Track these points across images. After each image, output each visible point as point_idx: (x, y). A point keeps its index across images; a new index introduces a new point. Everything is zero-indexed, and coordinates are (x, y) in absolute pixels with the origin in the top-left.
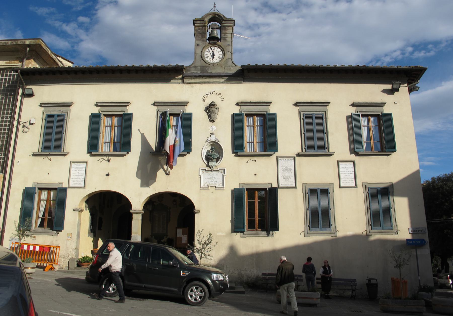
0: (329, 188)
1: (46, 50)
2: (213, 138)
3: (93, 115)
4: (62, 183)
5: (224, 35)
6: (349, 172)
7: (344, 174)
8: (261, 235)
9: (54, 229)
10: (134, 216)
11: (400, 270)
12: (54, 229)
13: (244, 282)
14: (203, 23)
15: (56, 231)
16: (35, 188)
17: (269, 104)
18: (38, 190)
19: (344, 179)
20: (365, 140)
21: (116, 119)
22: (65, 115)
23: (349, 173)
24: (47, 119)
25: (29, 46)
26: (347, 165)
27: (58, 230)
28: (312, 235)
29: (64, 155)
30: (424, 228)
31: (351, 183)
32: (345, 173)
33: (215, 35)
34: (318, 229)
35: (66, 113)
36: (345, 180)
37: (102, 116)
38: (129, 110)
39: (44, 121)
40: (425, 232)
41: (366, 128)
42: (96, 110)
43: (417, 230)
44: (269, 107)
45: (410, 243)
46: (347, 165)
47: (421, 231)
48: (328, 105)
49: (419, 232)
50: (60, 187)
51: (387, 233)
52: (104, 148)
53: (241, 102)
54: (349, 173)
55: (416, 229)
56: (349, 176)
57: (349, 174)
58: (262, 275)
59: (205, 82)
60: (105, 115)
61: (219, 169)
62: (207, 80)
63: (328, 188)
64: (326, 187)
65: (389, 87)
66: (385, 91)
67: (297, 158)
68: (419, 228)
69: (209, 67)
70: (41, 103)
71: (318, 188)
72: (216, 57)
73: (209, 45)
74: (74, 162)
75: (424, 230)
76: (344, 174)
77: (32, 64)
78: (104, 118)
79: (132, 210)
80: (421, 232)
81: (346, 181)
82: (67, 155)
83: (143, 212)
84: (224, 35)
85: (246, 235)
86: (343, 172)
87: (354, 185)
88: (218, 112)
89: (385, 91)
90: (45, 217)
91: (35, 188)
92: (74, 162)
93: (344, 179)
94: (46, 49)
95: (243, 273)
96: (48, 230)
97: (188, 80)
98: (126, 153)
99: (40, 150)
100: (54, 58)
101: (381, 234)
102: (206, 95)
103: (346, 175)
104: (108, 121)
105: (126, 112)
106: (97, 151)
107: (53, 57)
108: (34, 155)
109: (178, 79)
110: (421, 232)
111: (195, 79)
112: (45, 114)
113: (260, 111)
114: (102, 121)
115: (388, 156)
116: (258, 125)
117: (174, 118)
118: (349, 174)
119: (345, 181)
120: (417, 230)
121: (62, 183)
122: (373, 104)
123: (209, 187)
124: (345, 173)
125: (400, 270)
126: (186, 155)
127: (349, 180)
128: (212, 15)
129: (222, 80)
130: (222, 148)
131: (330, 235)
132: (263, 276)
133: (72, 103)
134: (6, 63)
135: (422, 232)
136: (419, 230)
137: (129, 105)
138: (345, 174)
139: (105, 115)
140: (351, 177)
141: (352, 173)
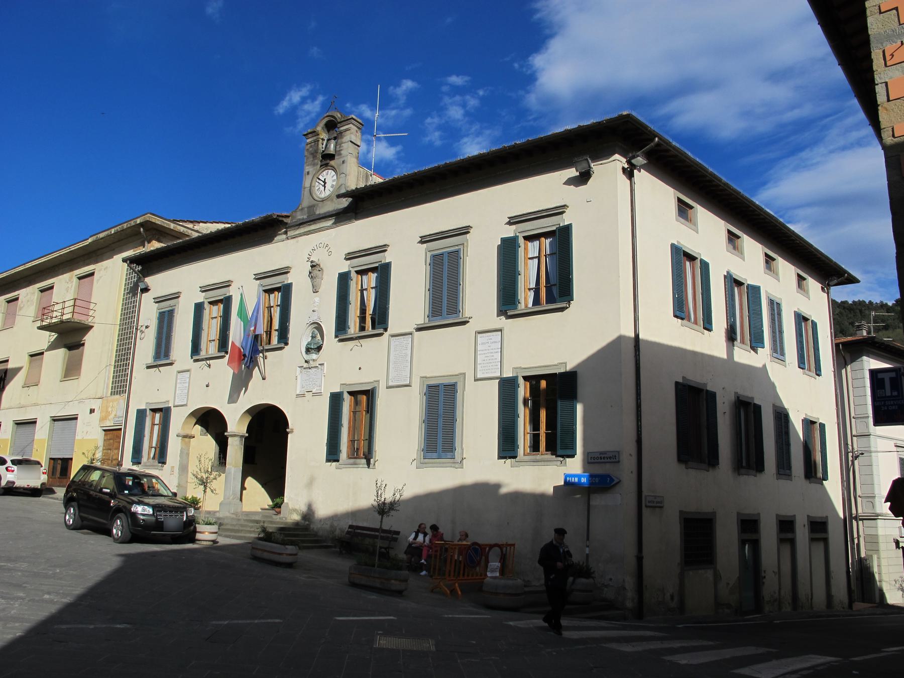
0: (457, 382)
1: (162, 224)
2: (314, 318)
3: (504, 240)
4: (566, 363)
5: (340, 147)
6: (492, 349)
7: (484, 354)
8: (361, 466)
9: (558, 454)
10: (230, 440)
11: (382, 519)
12: (558, 454)
13: (337, 538)
14: (315, 136)
15: (562, 456)
16: (517, 377)
17: (286, 271)
18: (349, 396)
19: (483, 364)
20: (277, 328)
21: (547, 242)
22: (460, 251)
23: (492, 353)
24: (432, 264)
25: (141, 225)
26: (490, 338)
27: (565, 455)
28: (427, 465)
29: (464, 323)
30: (617, 451)
31: (493, 371)
32: (485, 352)
33: (330, 151)
34: (435, 455)
35: (461, 247)
36: (485, 365)
37: (521, 241)
38: (565, 219)
39: (428, 267)
40: (617, 460)
41: (536, 261)
42: (510, 232)
43: (603, 456)
44: (386, 253)
45: (573, 480)
46: (490, 338)
47: (610, 458)
48: (468, 232)
49: (606, 460)
50: (562, 371)
51: (546, 463)
52: (526, 298)
53: (348, 253)
54: (492, 353)
55: (600, 454)
56: (493, 358)
57: (492, 355)
58: (349, 528)
59: (310, 231)
60: (526, 238)
61: (318, 365)
62: (313, 227)
63: (455, 383)
64: (452, 381)
65: (572, 172)
66: (571, 182)
67: (416, 334)
68: (605, 453)
69: (318, 205)
70: (509, 218)
71: (440, 384)
72: (328, 186)
73: (320, 170)
74: (480, 333)
75: (615, 456)
76: (484, 354)
77: (155, 245)
78: (525, 243)
79: (227, 432)
80: (609, 460)
81: (486, 368)
82: (468, 322)
83: (247, 435)
84: (340, 147)
85: (343, 466)
86: (483, 350)
87: (479, 376)
88: (322, 275)
89: (571, 182)
90: (534, 434)
91: (517, 377)
92: (480, 333)
93: (483, 364)
94: (164, 223)
95: (335, 524)
96: (549, 456)
97: (292, 232)
98: (381, 331)
99: (427, 319)
100: (184, 231)
101: (535, 464)
102: (312, 251)
103: (487, 357)
104: (533, 248)
105: (561, 225)
106: (346, 333)
107: (182, 231)
108: (148, 367)
109: (281, 234)
110: (609, 460)
111: (299, 229)
112: (429, 255)
113: (374, 262)
114: (521, 251)
115: (562, 311)
116: (279, 303)
117: (547, 240)
118: (492, 355)
119: (484, 368)
120: (601, 455)
121: (566, 363)
122: (543, 213)
123: (306, 393)
124: (485, 352)
125: (382, 519)
126: (284, 348)
127: (490, 365)
128: (326, 118)
129: (330, 223)
130: (323, 331)
131: (453, 465)
132: (350, 530)
133: (564, 206)
134: (134, 251)
135: (612, 460)
136: (605, 456)
137: (291, 271)
138: (486, 355)
139: (211, 303)
140: (496, 359)
141: (497, 352)
